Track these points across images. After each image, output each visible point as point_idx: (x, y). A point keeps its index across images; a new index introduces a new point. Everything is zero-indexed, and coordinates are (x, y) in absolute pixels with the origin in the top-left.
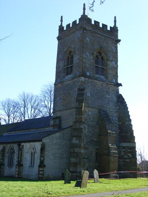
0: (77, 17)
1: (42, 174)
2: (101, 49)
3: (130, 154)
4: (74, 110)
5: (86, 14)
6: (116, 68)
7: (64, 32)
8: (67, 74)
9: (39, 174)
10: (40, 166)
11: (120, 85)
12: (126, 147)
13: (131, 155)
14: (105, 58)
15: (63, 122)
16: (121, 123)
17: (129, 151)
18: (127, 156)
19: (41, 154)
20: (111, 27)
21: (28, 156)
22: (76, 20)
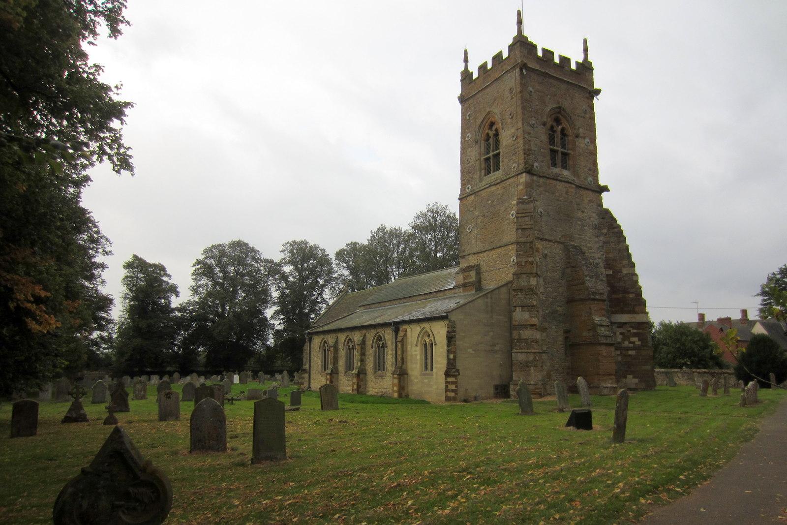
0: (502, 44)
1: (453, 391)
2: (559, 113)
3: (635, 339)
4: (514, 247)
5: (526, 33)
6: (593, 153)
7: (473, 84)
8: (488, 172)
9: (447, 390)
10: (447, 374)
11: (605, 189)
12: (625, 323)
13: (639, 340)
14: (569, 131)
15: (485, 276)
16: (611, 272)
17: (634, 333)
18: (630, 343)
19: (448, 346)
20: (577, 63)
21: (418, 353)
22: (501, 52)
